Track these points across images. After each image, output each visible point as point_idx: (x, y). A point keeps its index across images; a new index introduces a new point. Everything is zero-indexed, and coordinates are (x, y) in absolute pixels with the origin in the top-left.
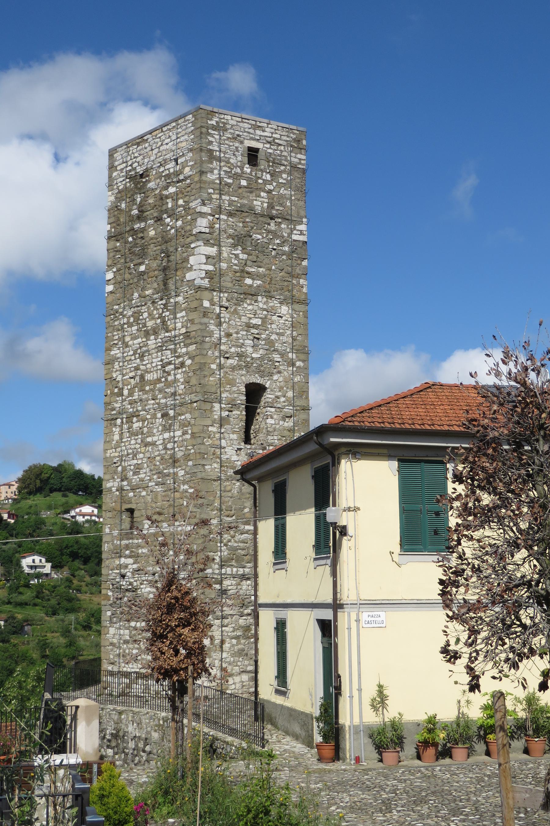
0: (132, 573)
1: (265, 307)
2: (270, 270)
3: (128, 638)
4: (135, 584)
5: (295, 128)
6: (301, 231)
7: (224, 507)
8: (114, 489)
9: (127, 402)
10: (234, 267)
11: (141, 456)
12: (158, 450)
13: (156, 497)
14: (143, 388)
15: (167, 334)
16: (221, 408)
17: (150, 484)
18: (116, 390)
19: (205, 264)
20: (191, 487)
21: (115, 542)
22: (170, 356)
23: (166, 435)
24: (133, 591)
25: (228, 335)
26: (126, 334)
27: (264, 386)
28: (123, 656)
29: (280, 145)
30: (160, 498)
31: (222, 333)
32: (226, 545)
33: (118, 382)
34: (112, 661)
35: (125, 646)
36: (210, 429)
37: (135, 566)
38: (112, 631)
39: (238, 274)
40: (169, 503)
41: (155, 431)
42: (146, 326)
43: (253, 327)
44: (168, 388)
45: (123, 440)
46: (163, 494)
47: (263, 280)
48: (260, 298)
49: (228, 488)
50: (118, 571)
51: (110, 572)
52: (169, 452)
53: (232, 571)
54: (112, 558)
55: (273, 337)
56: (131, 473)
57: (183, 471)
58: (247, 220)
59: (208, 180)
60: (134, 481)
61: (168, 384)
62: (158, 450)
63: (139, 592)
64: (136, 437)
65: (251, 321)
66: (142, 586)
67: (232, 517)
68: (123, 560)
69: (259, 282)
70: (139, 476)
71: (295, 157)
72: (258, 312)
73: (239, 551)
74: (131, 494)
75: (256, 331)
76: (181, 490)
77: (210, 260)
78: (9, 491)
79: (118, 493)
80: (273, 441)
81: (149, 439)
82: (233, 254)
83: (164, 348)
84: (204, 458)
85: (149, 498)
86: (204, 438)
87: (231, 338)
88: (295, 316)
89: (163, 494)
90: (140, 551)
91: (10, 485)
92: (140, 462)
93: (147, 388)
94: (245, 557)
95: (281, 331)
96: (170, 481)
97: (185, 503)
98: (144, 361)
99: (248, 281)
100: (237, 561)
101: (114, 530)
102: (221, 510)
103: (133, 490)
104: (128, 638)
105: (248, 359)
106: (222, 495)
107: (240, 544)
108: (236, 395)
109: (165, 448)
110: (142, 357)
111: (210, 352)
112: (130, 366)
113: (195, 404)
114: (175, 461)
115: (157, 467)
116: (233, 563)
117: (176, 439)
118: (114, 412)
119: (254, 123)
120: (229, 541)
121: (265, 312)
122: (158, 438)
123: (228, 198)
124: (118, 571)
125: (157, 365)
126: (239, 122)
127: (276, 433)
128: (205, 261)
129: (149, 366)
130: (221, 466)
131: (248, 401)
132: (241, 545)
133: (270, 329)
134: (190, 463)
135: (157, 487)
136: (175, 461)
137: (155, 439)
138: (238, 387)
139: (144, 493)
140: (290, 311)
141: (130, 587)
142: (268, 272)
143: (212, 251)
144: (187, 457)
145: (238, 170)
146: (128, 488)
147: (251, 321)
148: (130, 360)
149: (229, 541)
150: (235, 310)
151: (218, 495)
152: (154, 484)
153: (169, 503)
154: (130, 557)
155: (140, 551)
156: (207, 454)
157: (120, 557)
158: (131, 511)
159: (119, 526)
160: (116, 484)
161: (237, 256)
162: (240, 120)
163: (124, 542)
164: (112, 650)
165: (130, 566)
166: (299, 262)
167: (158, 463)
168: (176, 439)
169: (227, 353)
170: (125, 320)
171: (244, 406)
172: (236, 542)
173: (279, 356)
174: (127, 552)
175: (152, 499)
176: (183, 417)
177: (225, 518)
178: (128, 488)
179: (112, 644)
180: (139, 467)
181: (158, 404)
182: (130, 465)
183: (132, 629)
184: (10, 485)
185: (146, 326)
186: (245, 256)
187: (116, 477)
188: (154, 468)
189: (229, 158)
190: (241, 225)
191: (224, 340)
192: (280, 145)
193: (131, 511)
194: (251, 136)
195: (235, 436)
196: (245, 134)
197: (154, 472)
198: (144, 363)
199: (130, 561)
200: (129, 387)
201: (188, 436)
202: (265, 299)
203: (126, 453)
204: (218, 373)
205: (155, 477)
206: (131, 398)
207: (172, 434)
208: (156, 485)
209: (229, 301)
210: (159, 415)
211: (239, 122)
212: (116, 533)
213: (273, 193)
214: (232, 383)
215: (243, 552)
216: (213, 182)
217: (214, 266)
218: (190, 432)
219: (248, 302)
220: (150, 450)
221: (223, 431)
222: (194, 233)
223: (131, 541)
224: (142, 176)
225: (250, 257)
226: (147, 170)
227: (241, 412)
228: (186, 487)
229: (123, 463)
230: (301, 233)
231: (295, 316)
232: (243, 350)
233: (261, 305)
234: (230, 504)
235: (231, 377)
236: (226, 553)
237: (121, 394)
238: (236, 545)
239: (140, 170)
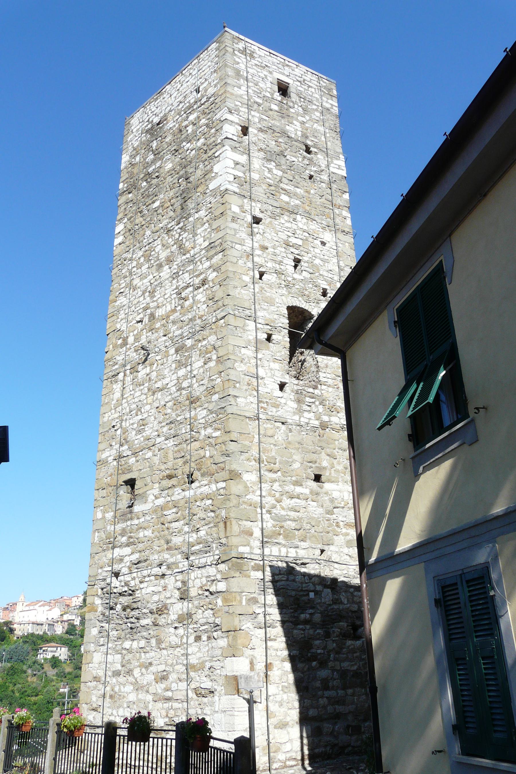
0: (129, 568)
1: (305, 228)
2: (308, 192)
3: (119, 667)
4: (132, 583)
5: (325, 77)
6: (339, 166)
7: (264, 457)
8: (110, 459)
9: (133, 350)
10: (268, 180)
11: (148, 407)
12: (171, 394)
13: (166, 456)
14: (153, 327)
15: (184, 257)
16: (257, 329)
17: (158, 440)
18: (120, 342)
19: (233, 168)
20: (217, 429)
21: (108, 528)
22: (187, 279)
23: (182, 372)
24: (130, 595)
25: (264, 248)
26: (135, 277)
27: (310, 313)
28: (111, 697)
29: (311, 87)
30: (171, 456)
31: (256, 245)
32: (269, 512)
33: (123, 331)
34: (95, 706)
35: (114, 680)
36: (243, 351)
37: (135, 557)
38: (98, 657)
39: (272, 188)
40: (184, 459)
41: (166, 372)
42: (158, 260)
43: (293, 246)
44: (185, 315)
45: (125, 396)
46: (176, 449)
47: (302, 200)
48: (299, 217)
49: (270, 433)
50: (110, 569)
51: (100, 571)
52: (184, 392)
53: (280, 551)
54: (104, 550)
55: (317, 262)
56: (134, 433)
57: (205, 411)
58: (280, 140)
59: (235, 93)
60: (136, 442)
61: (185, 311)
62: (171, 394)
63: (138, 594)
64: (142, 387)
65: (290, 240)
66: (142, 586)
67: (275, 472)
68: (117, 551)
69: (297, 202)
70: (144, 434)
71: (327, 102)
72: (298, 232)
73: (289, 523)
74: (132, 460)
75: (296, 252)
76: (201, 438)
77: (238, 166)
78: (77, 601)
79: (115, 463)
80: (325, 380)
81: (159, 385)
82: (266, 167)
83: (181, 273)
84: (235, 387)
85: (156, 460)
86: (235, 361)
87: (267, 251)
88: (341, 245)
89: (176, 449)
90: (141, 535)
91: (78, 597)
92: (145, 415)
93: (158, 325)
94: (296, 532)
95: (326, 257)
96: (184, 429)
97: (208, 454)
98: (155, 296)
99: (285, 198)
100: (286, 537)
101: (108, 512)
102: (259, 461)
103: (135, 454)
104: (119, 667)
105: (290, 279)
106: (262, 440)
107: (289, 513)
108: (276, 317)
109: (180, 389)
110: (152, 294)
111: (240, 262)
112: (137, 309)
113: (222, 321)
114: (193, 401)
115: (167, 417)
116: (281, 539)
117: (195, 373)
118: (116, 367)
119: (283, 61)
120: (274, 507)
121: (306, 234)
122: (170, 380)
123: (258, 115)
124: (110, 569)
125: (171, 295)
126: (267, 55)
127: (328, 370)
128: (233, 166)
129: (160, 300)
130: (259, 402)
131: (292, 325)
132: (293, 514)
133: (314, 253)
134: (216, 397)
135: (166, 442)
136: (193, 401)
137: (165, 381)
138: (278, 307)
139: (149, 454)
140: (334, 239)
141: (126, 589)
142: (307, 194)
143: (243, 159)
144: (211, 391)
145: (268, 95)
146: (129, 453)
147: (290, 240)
148: (139, 302)
149: (274, 507)
150: (270, 222)
151: (256, 440)
152: (163, 438)
153: (184, 459)
154: (128, 545)
155: (141, 535)
156: (239, 383)
157: (113, 548)
158: (131, 483)
159: (114, 506)
160: (114, 452)
161: (270, 170)
162: (268, 54)
163: (119, 527)
164: (95, 688)
165: (127, 559)
166: (340, 194)
167: (169, 411)
168: (195, 373)
169: (262, 266)
170: (134, 263)
171: (287, 331)
172: (283, 509)
173: (326, 283)
174: (124, 539)
175: (160, 459)
176: (204, 343)
177: (266, 473)
178: (129, 453)
179: (96, 679)
180: (144, 422)
181: (171, 339)
182: (133, 424)
183: (124, 652)
184: (78, 597)
185: (158, 260)
186: (280, 173)
187: (113, 444)
188: (164, 419)
189: (258, 82)
190: (274, 143)
191: (258, 252)
192: (311, 87)
193: (131, 483)
194: (280, 70)
195: (276, 366)
196: (274, 67)
197: (163, 424)
198: (155, 299)
199: (127, 550)
200: (136, 332)
201: (212, 364)
202: (305, 221)
203: (128, 410)
204: (252, 287)
205: (165, 429)
206: (137, 344)
207: (189, 368)
208: (166, 439)
209: (262, 212)
210: (172, 351)
211: (267, 55)
212: (110, 515)
213: (307, 125)
214: (271, 302)
215: (293, 525)
216: (241, 96)
217: (244, 174)
218: (214, 357)
219: (286, 218)
220: (159, 397)
221: (260, 356)
222: (219, 141)
223: (129, 523)
224: (158, 124)
225: (285, 175)
226: (165, 115)
227: (284, 336)
228: (209, 430)
229: (124, 424)
230: (339, 168)
231: (341, 245)
232: (282, 267)
233: (301, 225)
234: (273, 454)
235: (268, 294)
236: (270, 525)
237: (125, 343)
238: (283, 513)
239: (156, 120)
